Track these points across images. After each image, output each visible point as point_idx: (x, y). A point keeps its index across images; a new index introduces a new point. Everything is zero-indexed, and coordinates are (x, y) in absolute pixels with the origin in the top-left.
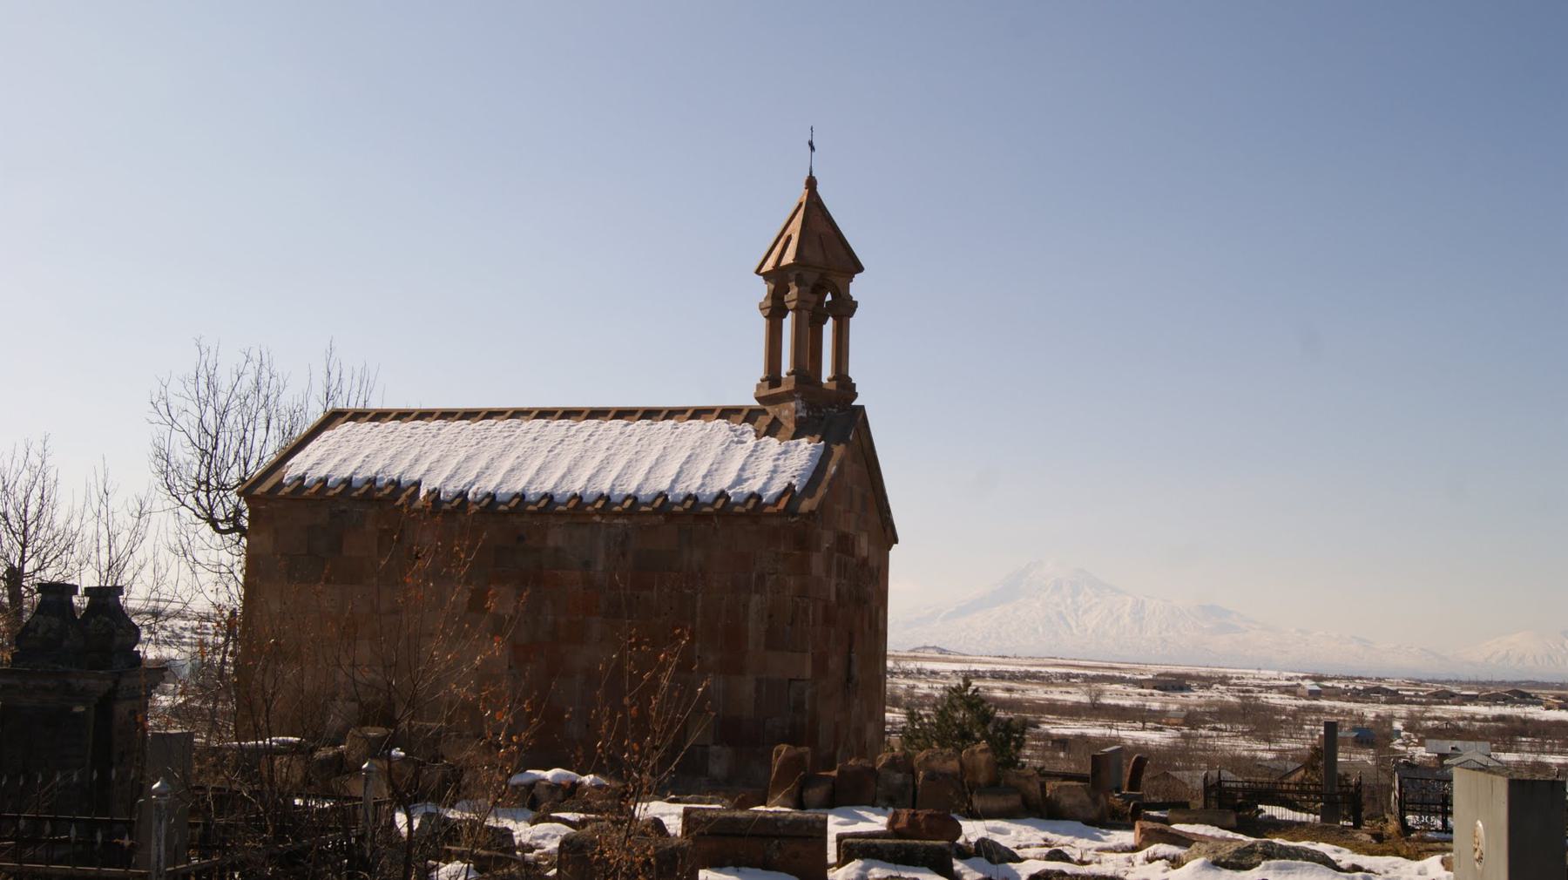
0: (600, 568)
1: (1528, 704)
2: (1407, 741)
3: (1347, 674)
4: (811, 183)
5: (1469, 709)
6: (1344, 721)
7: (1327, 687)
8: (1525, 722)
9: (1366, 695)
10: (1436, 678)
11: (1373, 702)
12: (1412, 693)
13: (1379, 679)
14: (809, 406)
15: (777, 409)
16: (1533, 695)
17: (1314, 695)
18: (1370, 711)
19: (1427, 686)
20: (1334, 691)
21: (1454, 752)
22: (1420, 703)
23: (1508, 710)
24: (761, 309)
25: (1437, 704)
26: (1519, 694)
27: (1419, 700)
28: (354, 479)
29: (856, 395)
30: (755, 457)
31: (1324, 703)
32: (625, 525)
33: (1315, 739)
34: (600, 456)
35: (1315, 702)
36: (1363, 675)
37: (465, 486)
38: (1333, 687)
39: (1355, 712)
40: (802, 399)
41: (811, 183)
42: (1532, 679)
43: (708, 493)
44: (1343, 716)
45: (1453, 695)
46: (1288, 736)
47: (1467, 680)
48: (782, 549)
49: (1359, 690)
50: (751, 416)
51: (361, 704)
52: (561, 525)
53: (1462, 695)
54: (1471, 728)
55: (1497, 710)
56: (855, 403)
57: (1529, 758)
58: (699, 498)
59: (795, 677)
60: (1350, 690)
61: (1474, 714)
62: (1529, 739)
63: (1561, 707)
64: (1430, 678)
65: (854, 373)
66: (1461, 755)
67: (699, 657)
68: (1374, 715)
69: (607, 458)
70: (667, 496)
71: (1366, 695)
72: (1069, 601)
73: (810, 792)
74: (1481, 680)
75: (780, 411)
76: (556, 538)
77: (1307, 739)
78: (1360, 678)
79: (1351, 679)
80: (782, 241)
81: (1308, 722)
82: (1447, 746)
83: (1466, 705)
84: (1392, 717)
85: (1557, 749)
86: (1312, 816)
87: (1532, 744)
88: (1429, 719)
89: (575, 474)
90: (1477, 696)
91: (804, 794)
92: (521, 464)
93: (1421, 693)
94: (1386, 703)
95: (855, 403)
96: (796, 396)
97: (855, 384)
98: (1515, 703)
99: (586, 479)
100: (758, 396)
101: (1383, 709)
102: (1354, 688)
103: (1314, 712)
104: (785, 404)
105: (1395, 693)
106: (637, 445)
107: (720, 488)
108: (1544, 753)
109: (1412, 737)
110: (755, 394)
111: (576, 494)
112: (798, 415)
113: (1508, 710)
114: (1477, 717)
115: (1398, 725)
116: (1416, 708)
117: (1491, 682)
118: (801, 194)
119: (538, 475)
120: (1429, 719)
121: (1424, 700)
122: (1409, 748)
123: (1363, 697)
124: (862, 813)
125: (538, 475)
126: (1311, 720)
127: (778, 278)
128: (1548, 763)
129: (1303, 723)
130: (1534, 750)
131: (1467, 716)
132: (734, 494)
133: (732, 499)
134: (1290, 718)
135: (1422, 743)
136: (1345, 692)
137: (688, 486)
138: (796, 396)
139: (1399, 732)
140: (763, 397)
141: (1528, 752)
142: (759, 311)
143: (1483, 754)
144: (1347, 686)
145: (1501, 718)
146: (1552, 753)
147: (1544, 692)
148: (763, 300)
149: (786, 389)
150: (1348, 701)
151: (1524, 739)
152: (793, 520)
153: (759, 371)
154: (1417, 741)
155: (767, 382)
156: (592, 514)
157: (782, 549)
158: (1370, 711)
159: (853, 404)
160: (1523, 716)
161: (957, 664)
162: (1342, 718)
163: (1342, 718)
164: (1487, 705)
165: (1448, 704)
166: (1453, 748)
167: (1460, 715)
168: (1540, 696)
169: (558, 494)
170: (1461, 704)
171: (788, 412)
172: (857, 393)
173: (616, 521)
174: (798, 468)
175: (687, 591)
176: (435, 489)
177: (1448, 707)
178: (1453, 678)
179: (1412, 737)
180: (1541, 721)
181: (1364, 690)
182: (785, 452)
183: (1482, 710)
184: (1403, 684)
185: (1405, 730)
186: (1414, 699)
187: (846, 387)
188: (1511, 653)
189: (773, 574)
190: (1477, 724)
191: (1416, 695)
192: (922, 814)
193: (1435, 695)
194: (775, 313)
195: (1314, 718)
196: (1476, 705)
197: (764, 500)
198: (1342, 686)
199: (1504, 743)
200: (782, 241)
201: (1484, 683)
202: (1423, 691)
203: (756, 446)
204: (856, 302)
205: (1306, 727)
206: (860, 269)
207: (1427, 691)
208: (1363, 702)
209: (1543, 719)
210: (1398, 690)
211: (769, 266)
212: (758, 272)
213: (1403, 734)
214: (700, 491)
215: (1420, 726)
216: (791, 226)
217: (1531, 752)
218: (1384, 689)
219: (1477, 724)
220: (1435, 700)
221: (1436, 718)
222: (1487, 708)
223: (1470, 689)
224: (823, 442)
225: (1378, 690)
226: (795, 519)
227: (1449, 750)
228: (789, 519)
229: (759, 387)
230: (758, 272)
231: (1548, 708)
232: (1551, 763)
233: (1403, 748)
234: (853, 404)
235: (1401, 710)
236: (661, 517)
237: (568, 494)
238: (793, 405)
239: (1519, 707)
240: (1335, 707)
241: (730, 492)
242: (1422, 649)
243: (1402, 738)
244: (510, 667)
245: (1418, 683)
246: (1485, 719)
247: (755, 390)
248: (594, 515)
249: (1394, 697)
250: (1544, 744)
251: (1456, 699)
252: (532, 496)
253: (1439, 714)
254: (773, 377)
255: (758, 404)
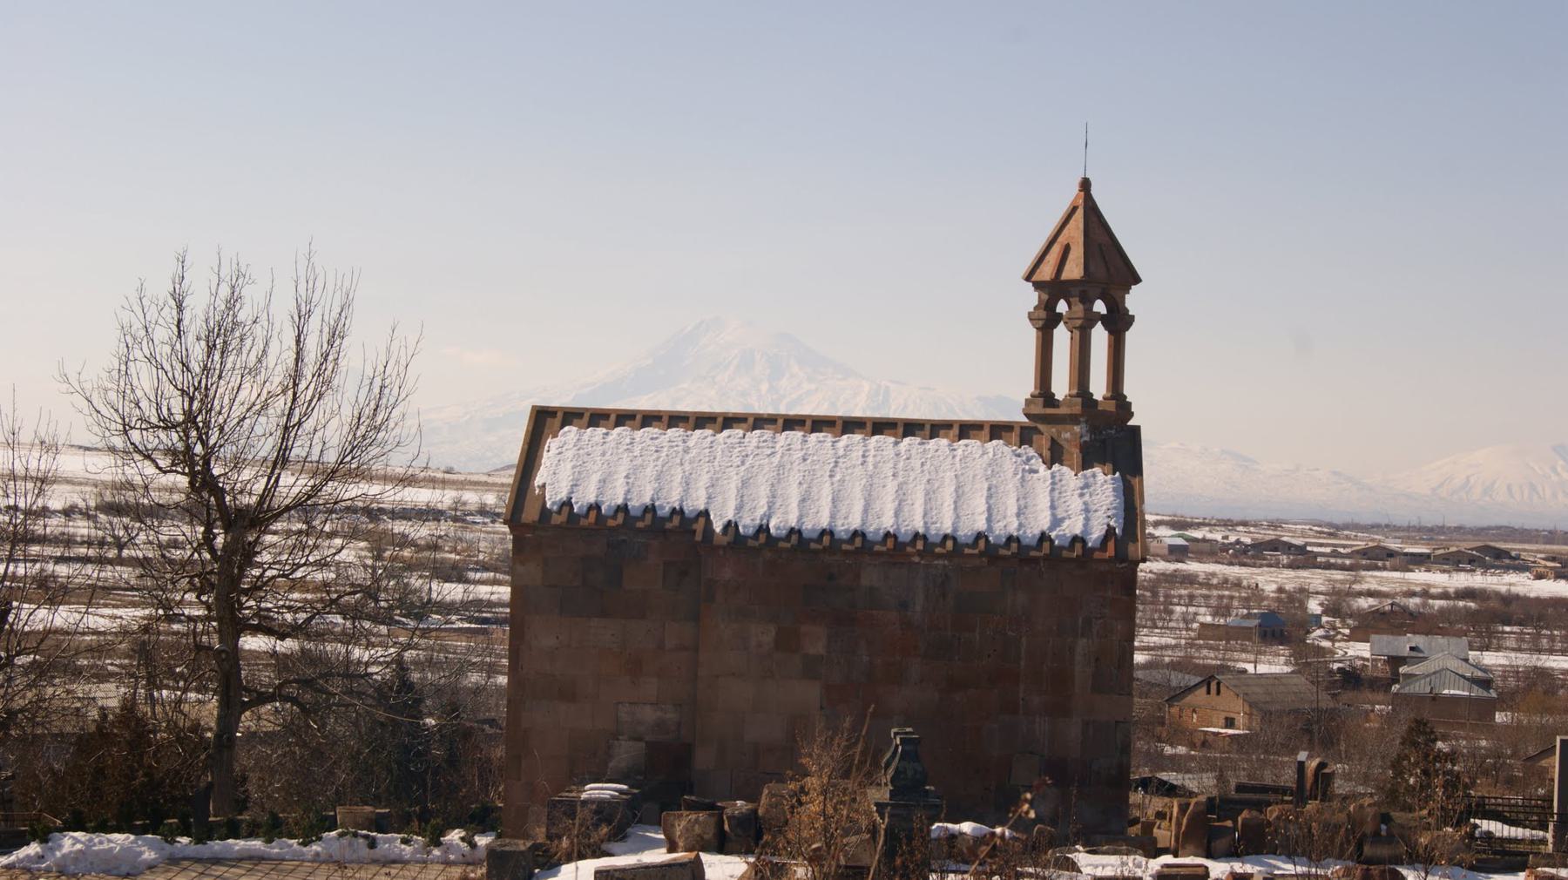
0: (918, 608)
1: (1507, 569)
2: (1332, 633)
3: (1226, 515)
4: (1085, 185)
5: (1419, 577)
6: (1232, 598)
7: (1196, 540)
8: (1509, 599)
9: (1254, 553)
10: (1357, 520)
11: (1270, 566)
12: (1328, 550)
13: (1274, 525)
14: (1093, 429)
15: (1054, 430)
16: (1513, 554)
17: (1177, 553)
18: (1270, 580)
19: (1348, 538)
20: (1206, 546)
21: (1414, 654)
22: (1343, 568)
23: (1477, 580)
24: (1031, 319)
25: (1368, 568)
26: (1494, 557)
27: (1339, 561)
28: (630, 507)
29: (1132, 414)
30: (1057, 491)
31: (1193, 567)
32: (944, 566)
33: (1191, 630)
34: (892, 486)
35: (1180, 566)
36: (1250, 516)
37: (762, 520)
38: (1204, 540)
39: (1245, 583)
40: (1086, 422)
41: (1085, 185)
42: (1507, 524)
43: (1030, 535)
44: (1227, 589)
45: (1391, 554)
46: (1149, 623)
47: (1406, 524)
48: (1110, 594)
49: (1247, 546)
50: (1025, 436)
51: (646, 742)
52: (875, 565)
53: (1406, 554)
54: (1427, 611)
55: (1461, 580)
56: (1131, 423)
57: (1523, 660)
58: (1022, 539)
59: (1122, 720)
60: (1231, 544)
61: (1429, 586)
62: (1516, 629)
63: (1559, 576)
64: (1348, 519)
65: (1130, 390)
66: (1425, 658)
67: (1023, 699)
68: (1274, 587)
69: (900, 486)
70: (987, 537)
71: (1254, 553)
72: (764, 387)
73: (1218, 842)
74: (1423, 524)
75: (1059, 433)
76: (871, 577)
77: (1180, 630)
78: (1245, 524)
79: (1229, 524)
80: (1056, 250)
81: (1175, 600)
82: (1403, 644)
83: (1412, 571)
84: (1304, 592)
85: (1559, 645)
86: (1520, 830)
87: (1520, 638)
88: (1360, 594)
89: (877, 506)
90: (1428, 556)
91: (1213, 844)
92: (808, 491)
93: (1341, 550)
94: (1291, 566)
95: (1131, 423)
96: (1082, 419)
97: (1130, 403)
98: (1486, 567)
99: (892, 513)
100: (1026, 412)
101: (1290, 579)
102: (1238, 542)
103: (1181, 583)
104: (1068, 427)
105: (1301, 550)
106: (923, 471)
107: (1039, 529)
108: (1540, 651)
109: (1338, 625)
110: (1024, 410)
111: (889, 532)
112: (1082, 440)
113: (1477, 580)
114: (1433, 591)
115: (1314, 606)
116: (1338, 575)
117: (1443, 527)
118: (1072, 193)
119: (835, 507)
120: (1360, 594)
121: (1348, 562)
122: (1337, 645)
123: (1253, 557)
124: (1271, 861)
125: (835, 507)
126: (1180, 597)
127: (1052, 290)
128: (1547, 669)
129: (1168, 600)
130: (1525, 646)
131: (1418, 589)
132: (1057, 536)
133: (1056, 542)
134: (1148, 594)
135: (1358, 635)
136: (1225, 548)
137: (1005, 526)
138: (1082, 419)
139: (1319, 617)
140: (1034, 415)
141: (1513, 650)
142: (1028, 320)
143: (1457, 658)
144: (1226, 537)
145: (1468, 594)
146: (1551, 651)
147: (1527, 546)
148: (1032, 310)
149: (1069, 412)
150: (1231, 564)
151: (1507, 629)
152: (1120, 566)
153: (1028, 387)
154: (1347, 631)
155: (1041, 400)
156: (912, 555)
157: (1110, 594)
158: (1270, 580)
159: (1129, 423)
160: (1503, 589)
161: (1212, 687)
162: (1227, 593)
163: (1227, 593)
164: (1444, 571)
165: (1384, 568)
166: (1412, 649)
167: (1405, 589)
168: (1524, 555)
169: (871, 532)
170: (1405, 569)
171: (1072, 435)
172: (1133, 413)
173: (936, 562)
174: (1110, 506)
175: (1010, 633)
176: (730, 522)
177: (1385, 574)
178: (1384, 522)
179: (1338, 625)
180: (1529, 598)
181: (1253, 546)
182: (1086, 486)
183: (1439, 579)
184: (1311, 533)
185: (1326, 612)
186: (1332, 560)
187: (1125, 409)
188: (1472, 480)
189: (1100, 618)
190: (1438, 603)
191: (1335, 554)
192: (1375, 869)
193: (1364, 553)
194: (1046, 322)
195: (1184, 592)
196: (1428, 570)
197: (1090, 545)
198: (1218, 536)
199: (1479, 635)
200: (1056, 250)
201: (1431, 530)
202: (1344, 547)
203: (1053, 477)
204: (1133, 316)
205: (1178, 609)
206: (1137, 280)
207: (1352, 546)
208: (1254, 566)
209: (1532, 595)
210: (1307, 544)
211: (1046, 273)
212: (1028, 278)
213: (1324, 619)
214: (1021, 532)
215: (1349, 607)
216: (1065, 231)
217: (1519, 650)
218: (1285, 543)
219: (1438, 603)
220: (1364, 562)
221: (1370, 594)
222: (1446, 576)
223: (1415, 543)
224: (1118, 474)
225: (1276, 545)
226: (1123, 565)
227: (1406, 652)
228: (1117, 565)
229: (1028, 402)
230: (1028, 278)
231: (1539, 577)
232: (1553, 669)
233: (1326, 644)
234: (1129, 423)
235: (1316, 579)
236: (984, 559)
237: (881, 531)
238: (1077, 429)
239: (1493, 574)
240: (1213, 575)
241: (1053, 535)
242: (1335, 473)
243: (1323, 627)
244: (822, 708)
245: (1335, 530)
246: (1445, 596)
247: (1023, 406)
248: (913, 556)
249: (1302, 558)
250: (1537, 637)
251: (1396, 561)
252: (843, 533)
253: (1374, 586)
254: (1043, 390)
255: (1026, 420)
